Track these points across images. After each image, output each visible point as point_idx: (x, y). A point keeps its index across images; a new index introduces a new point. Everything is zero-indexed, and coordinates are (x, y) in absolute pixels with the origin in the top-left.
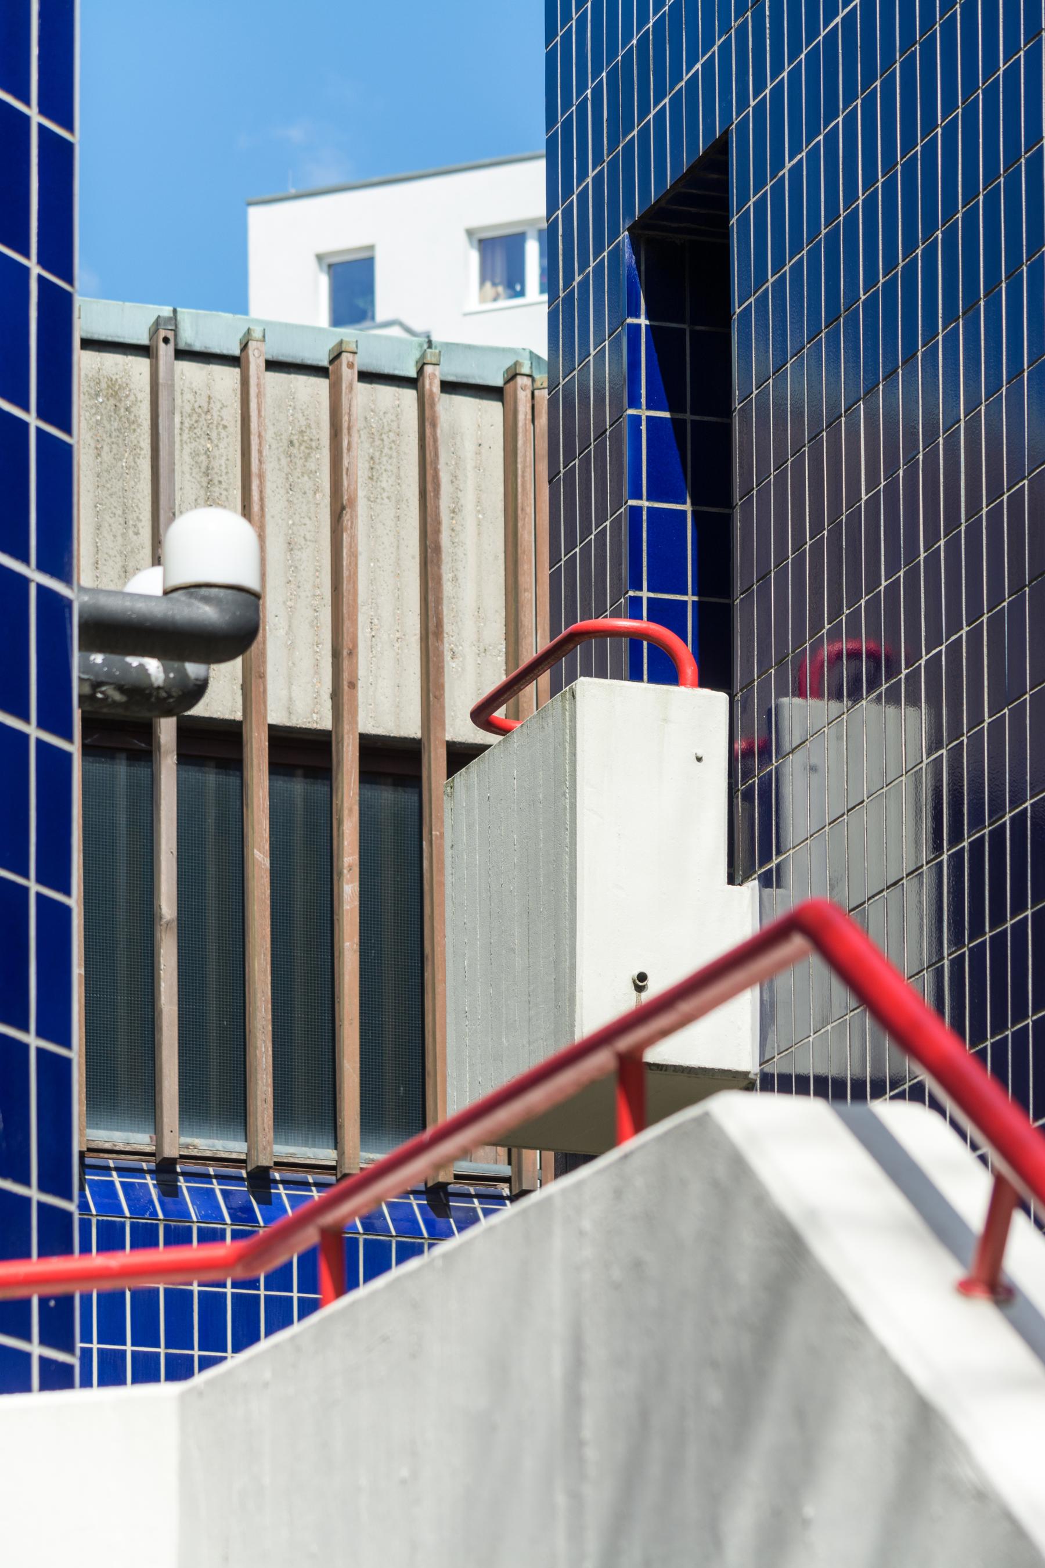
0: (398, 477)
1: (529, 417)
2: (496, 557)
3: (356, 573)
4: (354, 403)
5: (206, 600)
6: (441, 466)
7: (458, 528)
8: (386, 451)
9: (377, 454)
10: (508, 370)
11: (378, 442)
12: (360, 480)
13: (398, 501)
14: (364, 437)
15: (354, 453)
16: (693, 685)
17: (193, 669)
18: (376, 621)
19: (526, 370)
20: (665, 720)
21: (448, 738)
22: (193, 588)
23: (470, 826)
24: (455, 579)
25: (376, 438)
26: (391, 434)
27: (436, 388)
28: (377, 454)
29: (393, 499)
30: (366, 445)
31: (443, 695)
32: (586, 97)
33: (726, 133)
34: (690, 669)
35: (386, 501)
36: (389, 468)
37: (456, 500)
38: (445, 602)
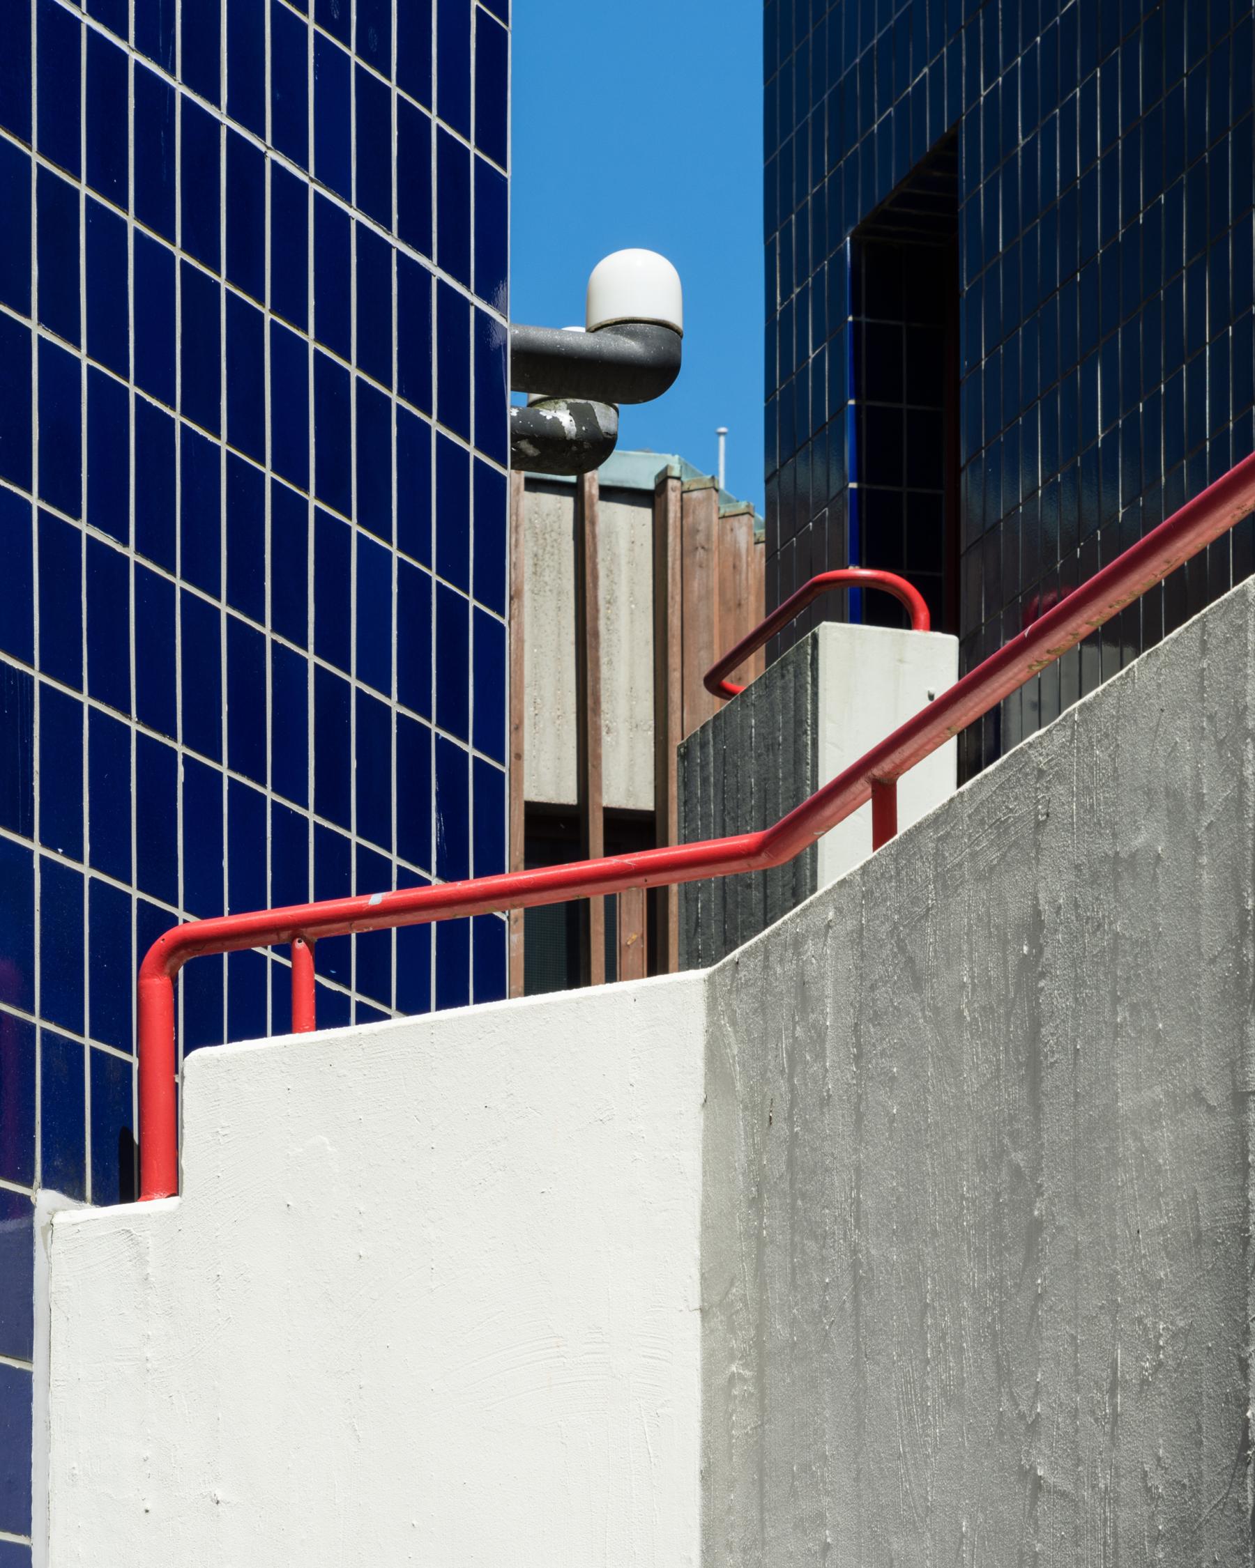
0: (559, 572)
1: (679, 515)
2: (647, 643)
3: (522, 657)
4: (521, 504)
5: (632, 335)
6: (599, 559)
7: (613, 617)
8: (548, 548)
9: (540, 552)
10: (658, 476)
11: (541, 541)
12: (526, 575)
13: (559, 593)
14: (528, 537)
15: (521, 548)
16: (925, 629)
17: (605, 416)
18: (538, 701)
19: (676, 473)
20: (901, 661)
21: (604, 804)
22: (619, 325)
23: (705, 781)
24: (610, 662)
25: (540, 537)
26: (553, 534)
27: (595, 491)
28: (540, 552)
29: (555, 592)
30: (531, 544)
31: (600, 764)
32: (806, 122)
33: (955, 125)
34: (923, 615)
35: (548, 593)
36: (551, 564)
37: (611, 592)
38: (602, 682)
